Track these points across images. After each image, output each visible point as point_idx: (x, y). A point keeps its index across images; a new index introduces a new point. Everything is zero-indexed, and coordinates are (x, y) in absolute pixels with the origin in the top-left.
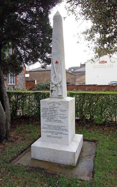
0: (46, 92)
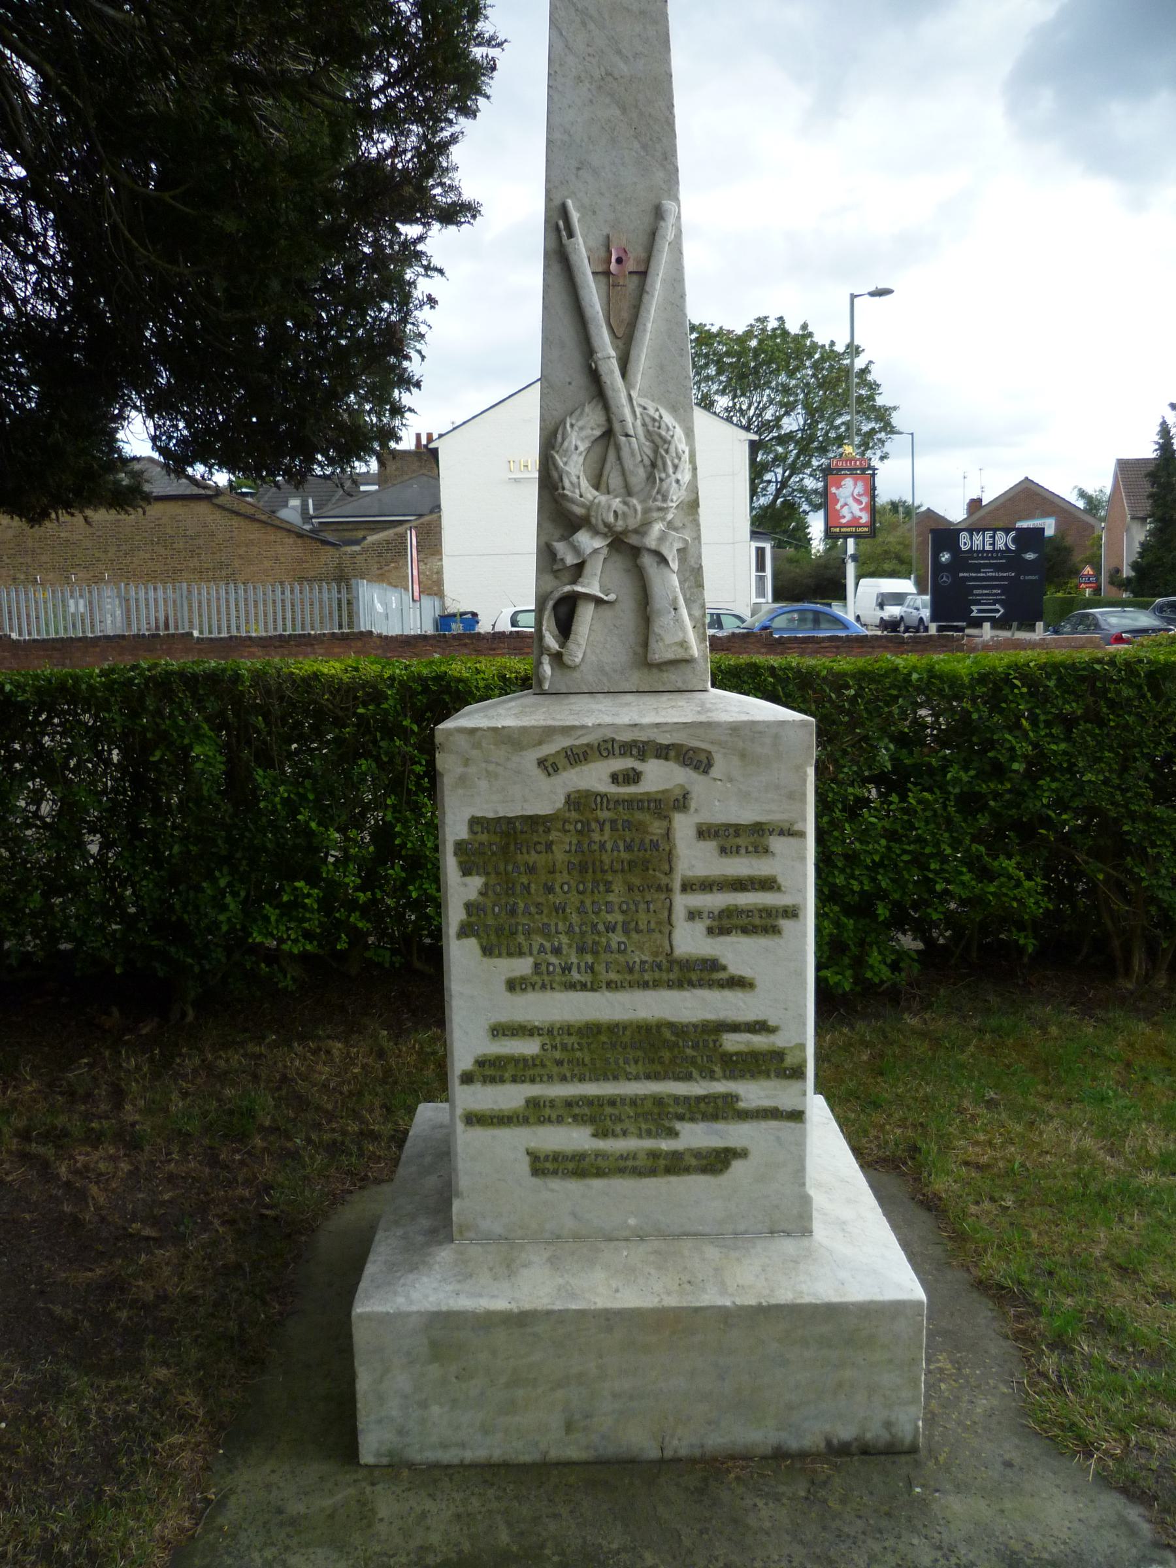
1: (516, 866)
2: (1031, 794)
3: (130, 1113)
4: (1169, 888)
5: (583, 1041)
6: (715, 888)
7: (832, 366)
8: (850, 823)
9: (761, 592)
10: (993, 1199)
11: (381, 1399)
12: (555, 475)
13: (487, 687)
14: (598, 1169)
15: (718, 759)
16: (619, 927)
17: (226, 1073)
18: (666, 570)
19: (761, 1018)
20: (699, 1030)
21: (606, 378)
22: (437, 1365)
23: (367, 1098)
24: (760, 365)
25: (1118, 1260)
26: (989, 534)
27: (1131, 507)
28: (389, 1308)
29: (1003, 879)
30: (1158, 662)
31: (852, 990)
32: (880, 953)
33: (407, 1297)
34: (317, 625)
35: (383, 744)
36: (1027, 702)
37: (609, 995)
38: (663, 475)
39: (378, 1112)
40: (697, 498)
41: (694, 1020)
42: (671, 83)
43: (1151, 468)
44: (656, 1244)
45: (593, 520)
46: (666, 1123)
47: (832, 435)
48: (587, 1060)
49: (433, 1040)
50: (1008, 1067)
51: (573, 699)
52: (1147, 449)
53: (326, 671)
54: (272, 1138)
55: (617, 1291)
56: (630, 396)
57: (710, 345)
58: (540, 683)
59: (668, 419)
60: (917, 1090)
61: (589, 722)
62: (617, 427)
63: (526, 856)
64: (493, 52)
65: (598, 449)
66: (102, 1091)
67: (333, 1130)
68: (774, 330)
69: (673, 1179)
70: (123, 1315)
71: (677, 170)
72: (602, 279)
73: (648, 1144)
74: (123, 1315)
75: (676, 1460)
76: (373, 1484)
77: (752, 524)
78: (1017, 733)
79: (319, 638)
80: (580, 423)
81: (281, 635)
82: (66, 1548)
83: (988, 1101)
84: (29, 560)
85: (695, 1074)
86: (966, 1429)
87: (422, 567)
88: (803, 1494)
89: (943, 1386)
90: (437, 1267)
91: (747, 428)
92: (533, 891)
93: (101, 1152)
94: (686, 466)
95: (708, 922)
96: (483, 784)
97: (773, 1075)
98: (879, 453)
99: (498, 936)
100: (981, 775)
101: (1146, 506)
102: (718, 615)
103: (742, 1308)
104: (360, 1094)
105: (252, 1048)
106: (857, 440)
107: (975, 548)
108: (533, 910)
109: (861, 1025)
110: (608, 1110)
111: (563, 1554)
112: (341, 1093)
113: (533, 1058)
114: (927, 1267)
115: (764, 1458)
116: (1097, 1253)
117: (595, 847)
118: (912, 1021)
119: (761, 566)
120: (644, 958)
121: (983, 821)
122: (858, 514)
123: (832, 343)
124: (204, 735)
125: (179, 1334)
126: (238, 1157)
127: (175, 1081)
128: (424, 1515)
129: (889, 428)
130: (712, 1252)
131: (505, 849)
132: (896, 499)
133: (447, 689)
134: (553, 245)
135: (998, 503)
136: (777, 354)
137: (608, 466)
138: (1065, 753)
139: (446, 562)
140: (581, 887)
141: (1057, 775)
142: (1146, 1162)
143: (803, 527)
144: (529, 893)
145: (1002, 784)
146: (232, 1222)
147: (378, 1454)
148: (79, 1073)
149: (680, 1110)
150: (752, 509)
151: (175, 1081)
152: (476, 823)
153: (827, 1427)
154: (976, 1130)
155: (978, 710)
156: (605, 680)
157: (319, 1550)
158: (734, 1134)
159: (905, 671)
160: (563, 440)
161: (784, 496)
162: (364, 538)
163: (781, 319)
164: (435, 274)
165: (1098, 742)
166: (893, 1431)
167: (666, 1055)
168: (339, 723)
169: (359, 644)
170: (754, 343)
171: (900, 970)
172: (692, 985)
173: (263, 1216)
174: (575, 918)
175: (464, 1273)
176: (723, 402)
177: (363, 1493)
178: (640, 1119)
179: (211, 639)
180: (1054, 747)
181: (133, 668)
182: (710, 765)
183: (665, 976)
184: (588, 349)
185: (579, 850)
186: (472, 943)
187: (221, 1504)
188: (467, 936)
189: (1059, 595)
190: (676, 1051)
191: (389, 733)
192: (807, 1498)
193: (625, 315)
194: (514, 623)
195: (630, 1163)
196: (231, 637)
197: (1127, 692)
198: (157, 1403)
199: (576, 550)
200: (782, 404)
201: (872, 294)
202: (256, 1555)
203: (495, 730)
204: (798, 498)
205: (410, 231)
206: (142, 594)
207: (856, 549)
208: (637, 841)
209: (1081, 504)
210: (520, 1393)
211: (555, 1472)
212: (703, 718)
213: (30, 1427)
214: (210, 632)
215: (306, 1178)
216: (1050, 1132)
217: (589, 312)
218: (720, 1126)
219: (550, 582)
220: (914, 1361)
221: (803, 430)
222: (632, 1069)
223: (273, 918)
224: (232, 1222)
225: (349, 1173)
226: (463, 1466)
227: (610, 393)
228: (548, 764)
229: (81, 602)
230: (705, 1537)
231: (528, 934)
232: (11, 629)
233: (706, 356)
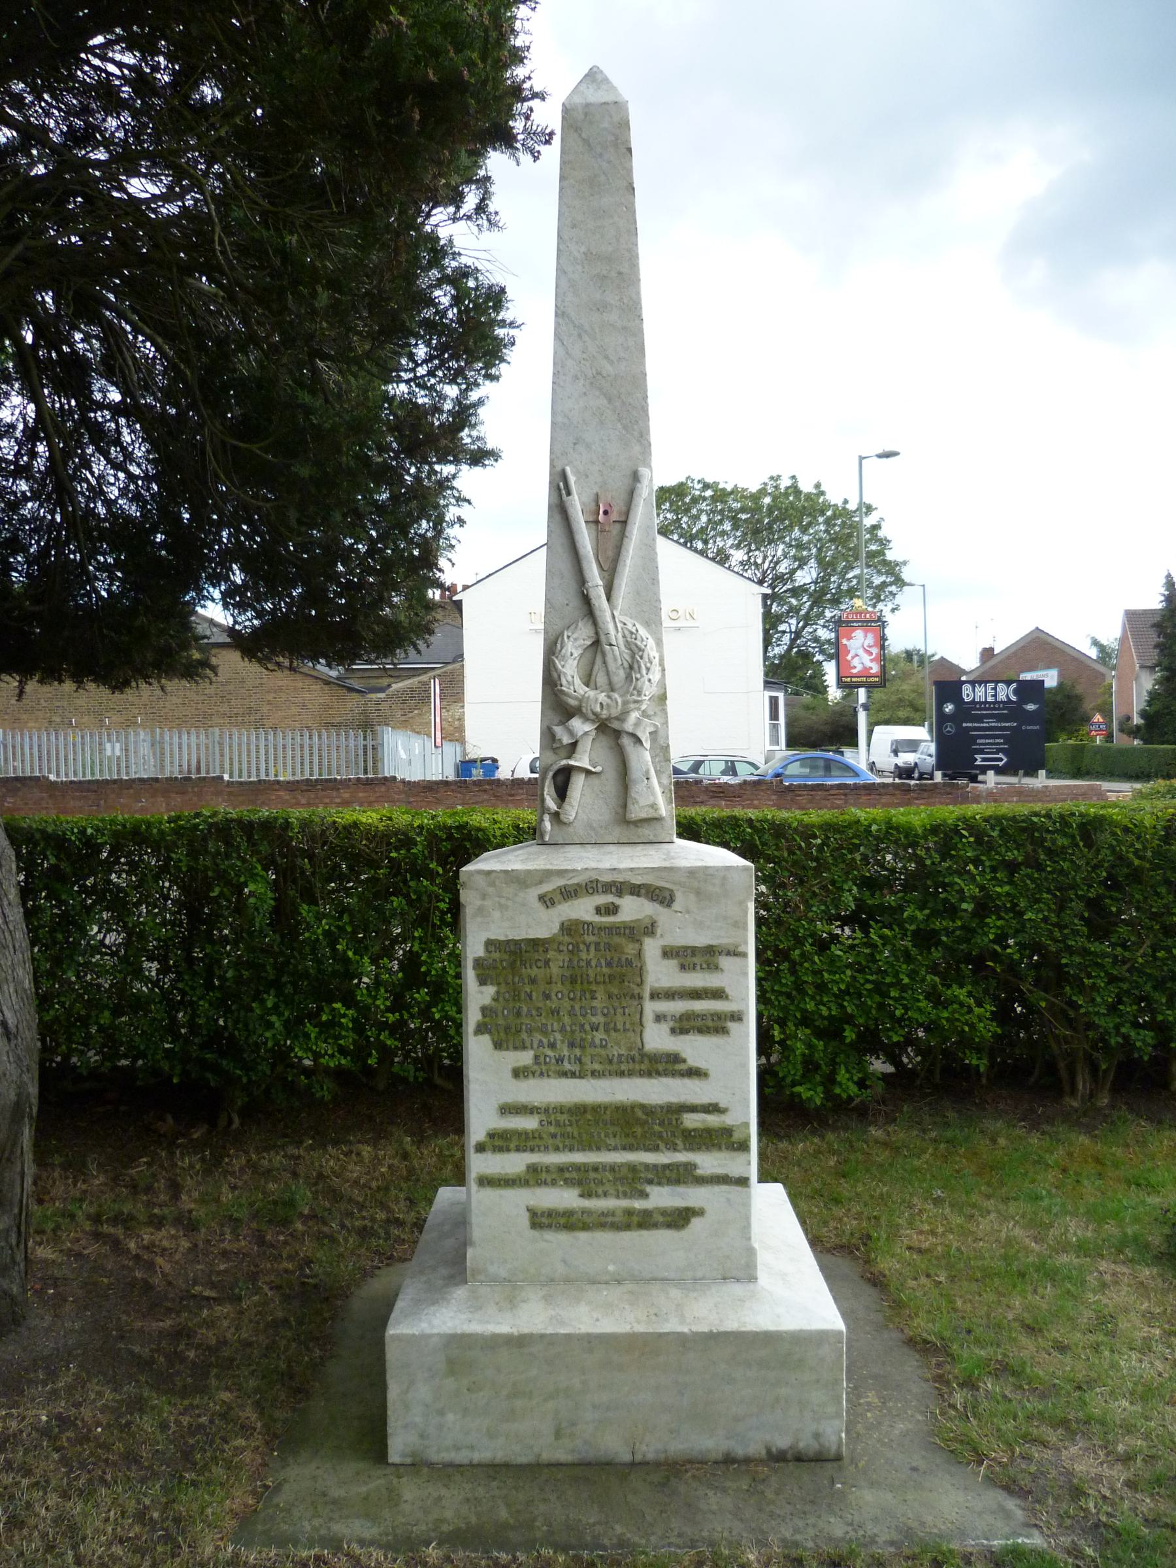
2: (980, 931)
3: (187, 1202)
4: (1104, 1015)
5: (573, 1119)
7: (844, 523)
8: (819, 956)
9: (775, 740)
10: (928, 1276)
11: (407, 1407)
12: (555, 675)
13: (503, 836)
14: (584, 1223)
16: (601, 1028)
17: (269, 1171)
18: (640, 748)
19: (714, 1101)
21: (594, 601)
22: (453, 1379)
23: (393, 1192)
24: (774, 521)
25: (1027, 1322)
26: (990, 686)
27: (1139, 657)
28: (415, 1331)
29: (955, 1006)
30: (1088, 815)
31: (822, 1105)
32: (847, 1071)
33: (430, 1323)
34: (343, 770)
35: (412, 884)
36: (975, 850)
37: (594, 1082)
39: (402, 1204)
41: (660, 1102)
42: (645, 380)
43: (1157, 619)
44: (629, 1286)
45: (584, 710)
46: (639, 1187)
47: (845, 587)
48: (576, 1134)
49: (451, 1145)
50: (958, 1172)
51: (568, 848)
52: (1153, 600)
53: (364, 820)
54: (310, 1223)
55: (597, 1320)
56: (614, 617)
57: (724, 502)
58: (542, 836)
59: (643, 632)
60: (875, 1190)
62: (603, 638)
64: (512, 332)
65: (589, 655)
66: (161, 1184)
67: (364, 1218)
68: (787, 488)
69: (644, 1233)
70: (192, 1354)
71: (650, 445)
72: (593, 526)
73: (625, 1203)
75: (644, 1463)
76: (399, 1477)
77: (766, 675)
78: (966, 877)
79: (345, 783)
80: (575, 636)
81: (307, 780)
82: (156, 1515)
84: (65, 704)
85: (662, 1145)
86: (884, 1444)
87: (445, 714)
88: (745, 1487)
89: (869, 1415)
91: (761, 582)
92: (534, 997)
93: (163, 1232)
94: (656, 668)
95: (671, 1024)
96: (497, 914)
98: (890, 606)
100: (935, 914)
101: (1153, 656)
102: (733, 762)
104: (387, 1189)
105: (292, 1150)
106: (870, 592)
107: (977, 699)
108: (534, 1012)
109: (830, 1136)
110: (592, 1175)
111: (550, 1525)
112: (370, 1188)
113: (533, 1132)
114: (868, 1328)
115: (716, 1462)
116: (1010, 1317)
117: (583, 964)
118: (875, 1132)
119: (774, 715)
120: (622, 1052)
121: (936, 954)
122: (868, 664)
123: (846, 502)
124: (257, 875)
125: (238, 1368)
126: (282, 1238)
127: (225, 1177)
128: (440, 1498)
129: (900, 582)
130: (675, 1293)
131: (512, 965)
132: (910, 647)
133: (469, 837)
134: (556, 501)
135: (1008, 653)
136: (791, 511)
137: (596, 667)
138: (1008, 894)
139: (466, 709)
140: (572, 995)
141: (1003, 914)
142: (1064, 1247)
143: (819, 674)
144: (531, 999)
145: (954, 922)
146: (278, 1288)
147: (404, 1455)
148: (140, 1169)
149: (650, 1176)
150: (766, 658)
151: (225, 1177)
152: (490, 944)
154: (922, 1222)
155: (931, 857)
157: (357, 1521)
158: (692, 1196)
159: (866, 823)
160: (562, 648)
161: (798, 646)
162: (389, 686)
163: (793, 477)
164: (466, 504)
165: (1038, 886)
168: (374, 865)
169: (383, 789)
170: (767, 500)
171: (866, 1087)
172: (659, 1074)
173: (303, 1283)
174: (567, 1020)
175: (475, 1305)
176: (738, 556)
179: (241, 783)
180: (998, 889)
181: (197, 815)
183: (637, 1067)
184: (581, 580)
186: (486, 1039)
187: (278, 1488)
188: (482, 1033)
189: (1071, 742)
190: (646, 1128)
191: (417, 875)
193: (610, 553)
195: (610, 1219)
196: (260, 781)
197: (1062, 841)
198: (224, 1416)
199: (571, 733)
200: (795, 558)
201: (880, 456)
202: (306, 1523)
203: (506, 872)
204: (812, 647)
205: (447, 470)
206: (176, 739)
207: (869, 697)
208: (616, 959)
209: (1093, 653)
210: (519, 1403)
211: (546, 1471)
212: (667, 864)
213: (122, 1431)
214: (240, 776)
215: (341, 1255)
216: (985, 1225)
217: (582, 551)
218: (681, 1189)
219: (550, 757)
220: (837, 1382)
221: (816, 582)
222: (611, 1142)
223: (313, 1036)
224: (278, 1288)
225: (377, 1252)
226: (472, 1465)
227: (597, 613)
229: (118, 745)
231: (530, 1032)
232: (49, 772)
233: (721, 512)
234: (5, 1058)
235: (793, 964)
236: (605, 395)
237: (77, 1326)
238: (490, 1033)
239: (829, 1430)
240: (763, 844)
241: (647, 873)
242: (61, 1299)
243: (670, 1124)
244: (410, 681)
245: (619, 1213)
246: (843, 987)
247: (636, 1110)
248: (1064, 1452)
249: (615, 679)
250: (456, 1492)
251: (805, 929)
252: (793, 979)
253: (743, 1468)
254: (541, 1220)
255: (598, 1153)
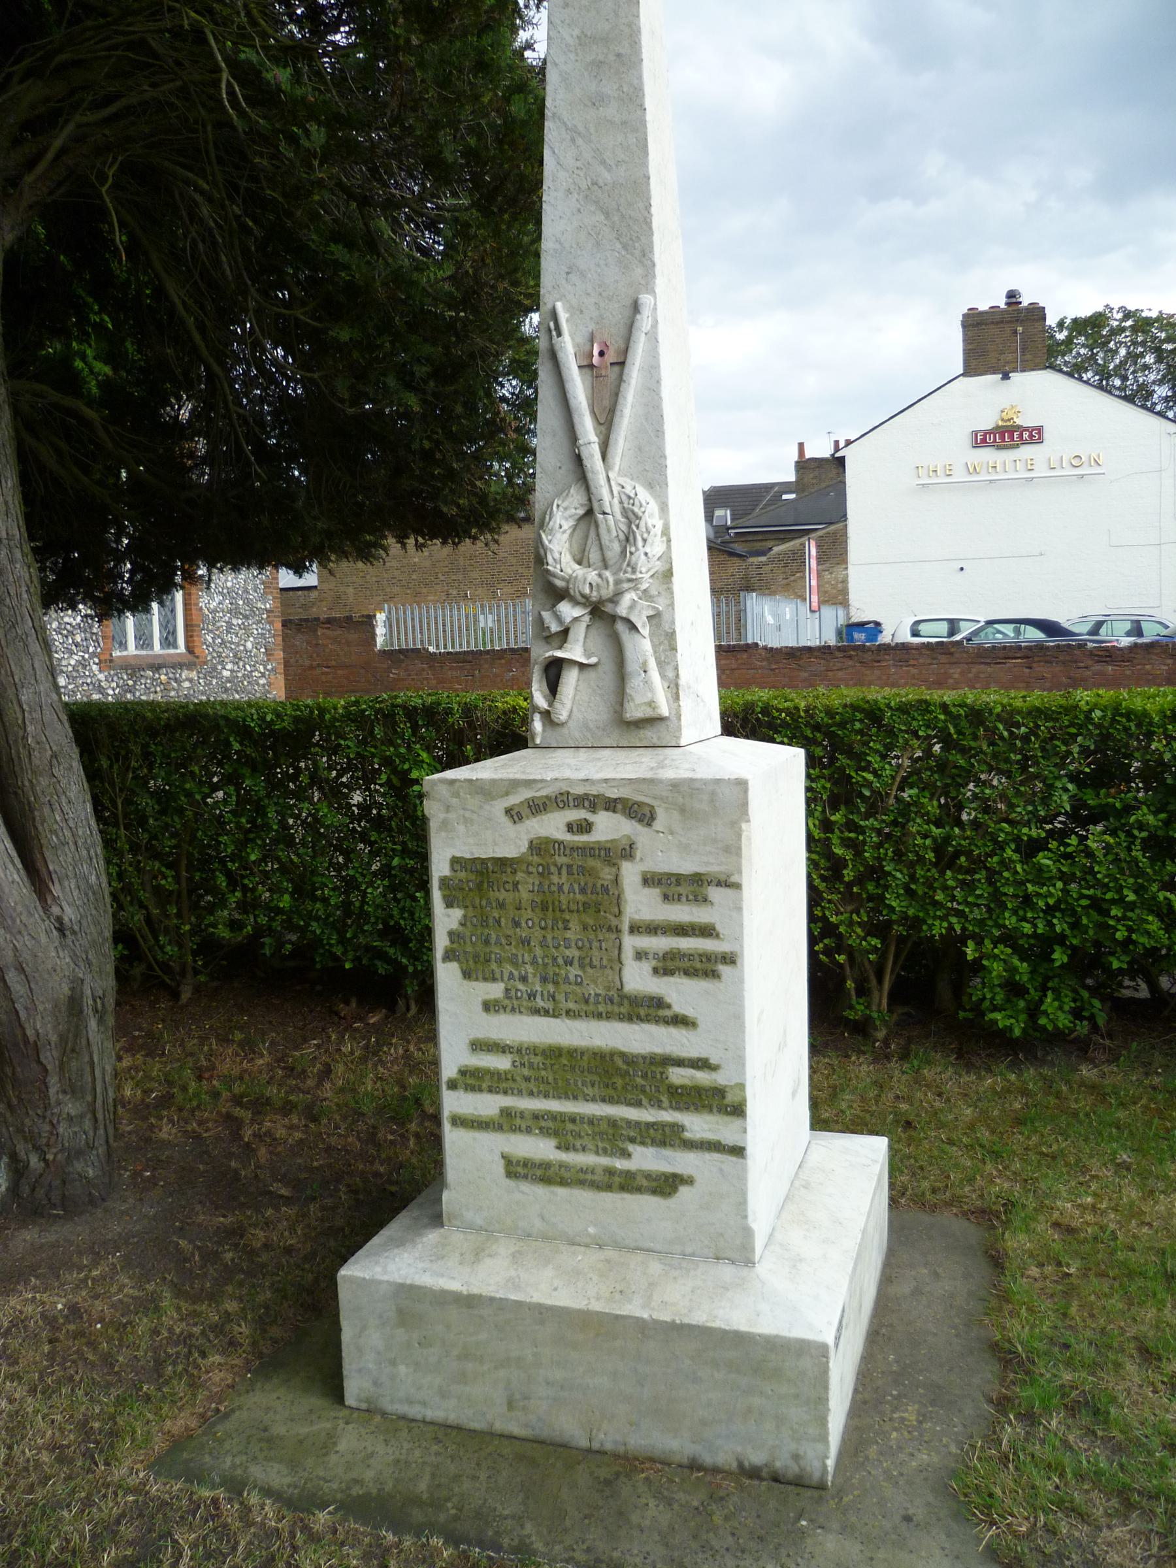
0: (527, 302)
1: (489, 902)
6: (659, 932)
15: (660, 813)
18: (637, 636)
19: (704, 1055)
20: (648, 1061)
21: (586, 462)
22: (403, 1330)
38: (633, 549)
40: (671, 568)
41: (643, 1052)
44: (610, 1253)
45: (572, 592)
48: (551, 1079)
55: (555, 1289)
59: (643, 495)
61: (549, 776)
63: (497, 893)
69: (627, 1196)
71: (654, 265)
72: (587, 370)
73: (605, 1161)
74: (229, 1256)
75: (601, 1453)
80: (565, 504)
83: (1118, 1165)
84: (461, 577)
85: (645, 1101)
88: (695, 1503)
90: (420, 1246)
92: (503, 924)
95: (654, 963)
96: (461, 828)
97: (715, 1110)
99: (476, 962)
102: (1138, 622)
103: (656, 1322)
108: (503, 941)
110: (570, 1126)
111: (460, 1510)
114: (957, 1321)
115: (680, 1466)
117: (554, 888)
118: (1087, 1072)
124: (423, 761)
130: (655, 1267)
131: (479, 887)
137: (589, 542)
140: (543, 923)
144: (500, 926)
149: (632, 1134)
152: (455, 861)
153: (739, 1449)
156: (589, 735)
157: (276, 1466)
159: (1085, 708)
162: (771, 549)
166: (802, 1463)
167: (619, 1082)
169: (745, 656)
172: (640, 1019)
174: (538, 951)
177: (335, 1428)
178: (597, 1137)
182: (653, 818)
183: (616, 1009)
185: (541, 891)
186: (454, 967)
187: (227, 1416)
192: (697, 1509)
193: (606, 403)
194: (915, 634)
195: (589, 1177)
199: (558, 618)
203: (470, 781)
208: (590, 885)
210: (470, 1366)
217: (573, 403)
218: (667, 1152)
222: (589, 1091)
227: (589, 475)
228: (513, 813)
230: (587, 1521)
231: (500, 962)
232: (430, 644)
234: (54, 954)
235: (991, 873)
236: (601, 209)
237: (152, 1212)
238: (458, 961)
239: (810, 1454)
240: (959, 732)
241: (624, 785)
242: (153, 1181)
243: (654, 1077)
244: (792, 543)
245: (599, 1171)
246: (1051, 901)
247: (616, 1058)
248: (1105, 1532)
249: (609, 554)
250: (390, 1452)
251: (1007, 834)
252: (991, 889)
253: (709, 1478)
254: (517, 1169)
255: (575, 1103)
